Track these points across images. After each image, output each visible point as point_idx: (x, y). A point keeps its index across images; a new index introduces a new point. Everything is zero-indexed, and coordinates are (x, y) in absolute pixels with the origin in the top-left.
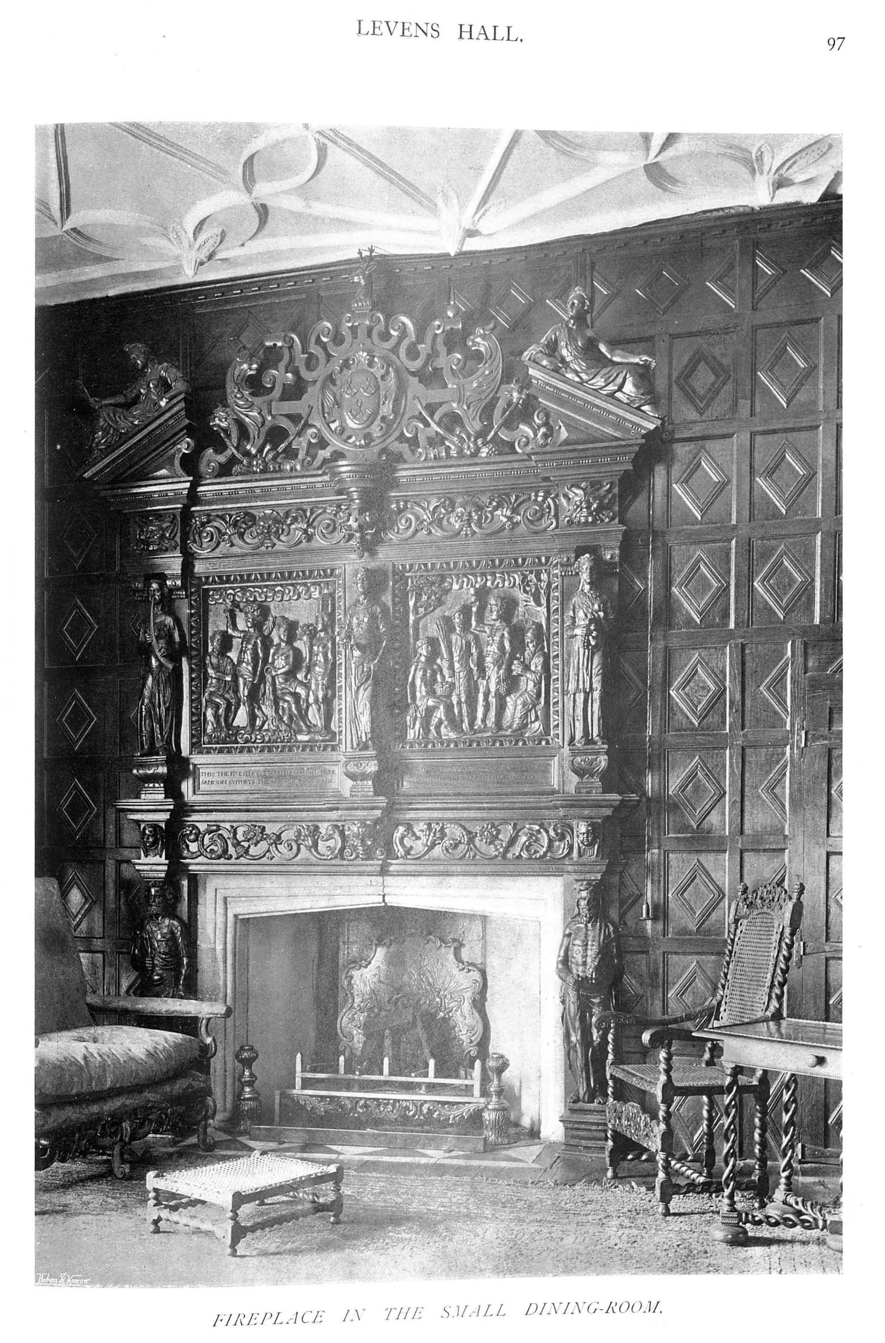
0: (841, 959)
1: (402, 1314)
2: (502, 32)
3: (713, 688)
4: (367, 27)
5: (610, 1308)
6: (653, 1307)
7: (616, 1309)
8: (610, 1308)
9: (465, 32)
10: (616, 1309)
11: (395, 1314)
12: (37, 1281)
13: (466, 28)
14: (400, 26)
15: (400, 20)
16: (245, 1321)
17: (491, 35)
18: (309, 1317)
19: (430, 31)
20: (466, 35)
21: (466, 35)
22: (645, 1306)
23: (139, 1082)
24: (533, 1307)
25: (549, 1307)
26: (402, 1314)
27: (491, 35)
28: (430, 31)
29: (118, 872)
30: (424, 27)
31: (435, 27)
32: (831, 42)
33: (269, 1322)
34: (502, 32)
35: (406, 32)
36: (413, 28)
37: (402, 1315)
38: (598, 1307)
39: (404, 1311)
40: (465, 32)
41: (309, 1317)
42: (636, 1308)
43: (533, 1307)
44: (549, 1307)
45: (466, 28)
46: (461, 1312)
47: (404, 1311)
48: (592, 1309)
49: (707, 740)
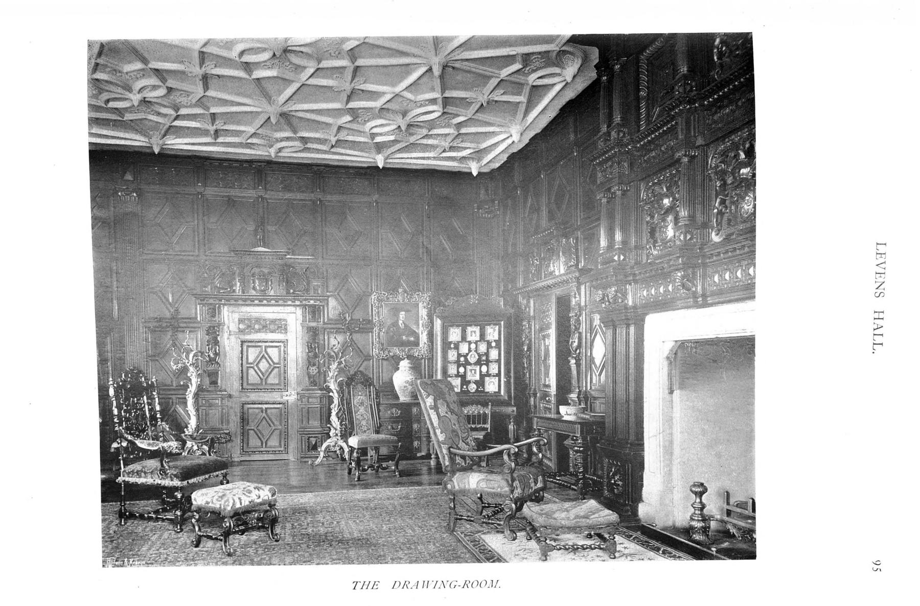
0: (93, 121)
1: (365, 585)
2: (878, 339)
4: (882, 249)
6: (493, 584)
7: (470, 585)
9: (879, 315)
10: (470, 585)
14: (883, 271)
15: (886, 271)
17: (877, 332)
19: (879, 291)
21: (876, 315)
24: (397, 584)
25: (439, 583)
26: (365, 585)
27: (877, 332)
28: (879, 291)
29: (564, 275)
34: (878, 339)
36: (881, 280)
37: (365, 587)
39: (367, 583)
40: (879, 315)
42: (483, 584)
43: (397, 584)
44: (439, 583)
46: (406, 584)
48: (452, 586)
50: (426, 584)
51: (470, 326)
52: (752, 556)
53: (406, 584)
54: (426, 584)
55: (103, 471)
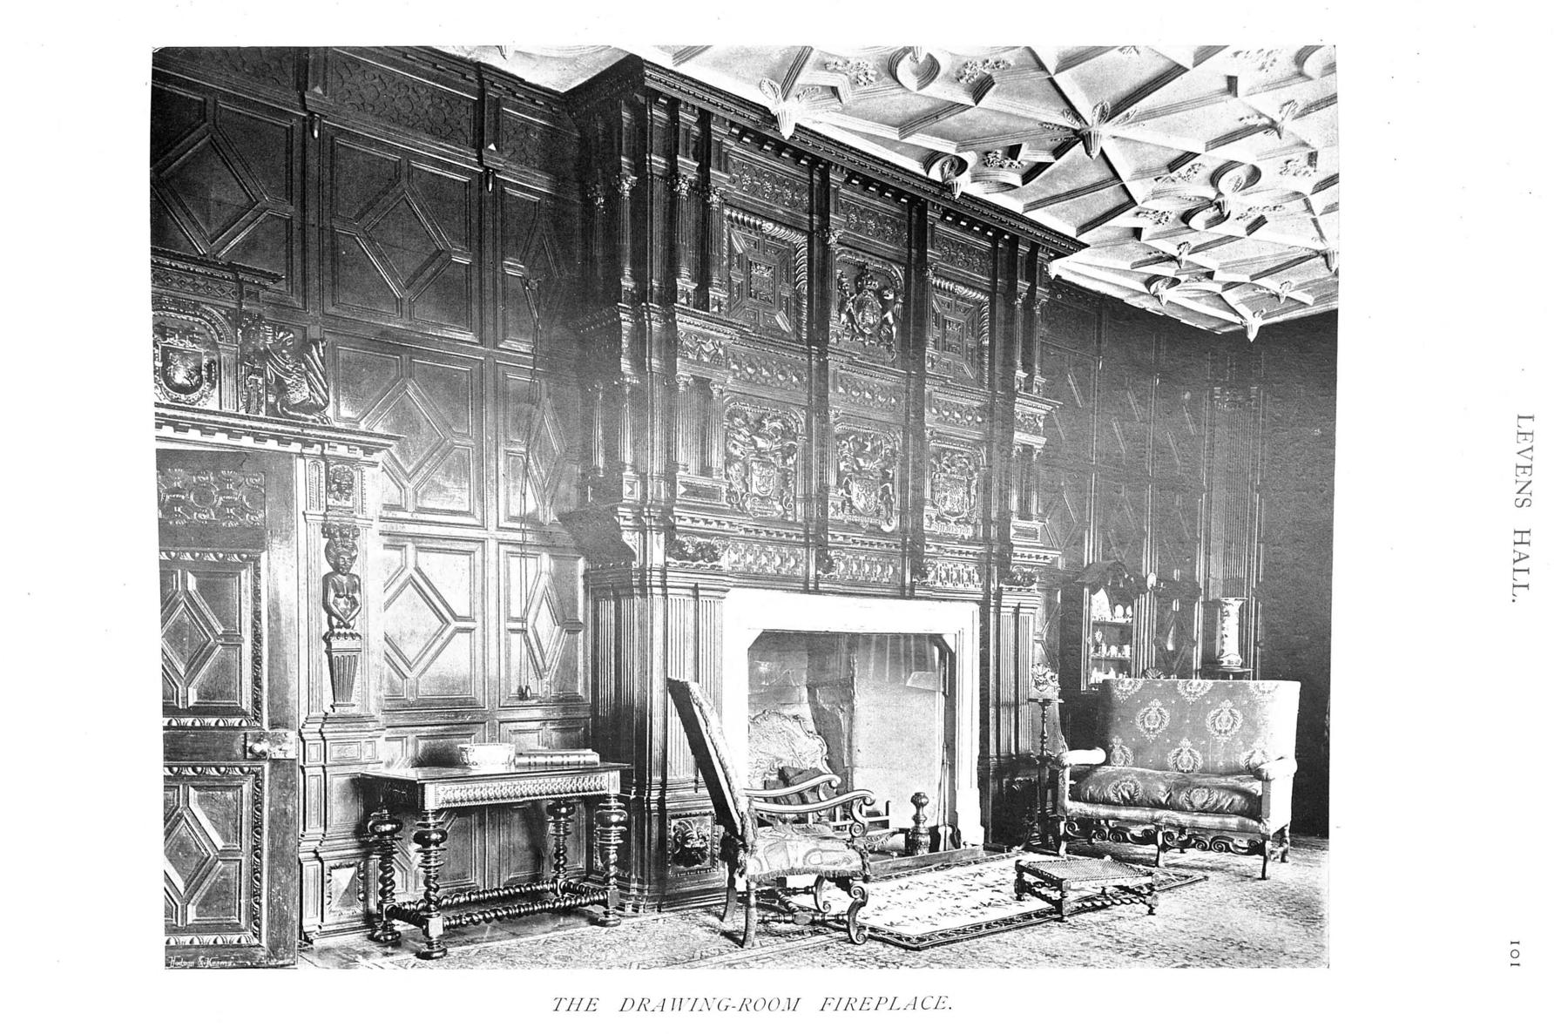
1: (574, 1005)
2: (1522, 578)
4: (1527, 426)
5: (744, 1005)
7: (751, 1007)
8: (744, 1005)
9: (1522, 536)
10: (751, 1007)
11: (565, 1005)
12: (168, 965)
13: (1526, 538)
16: (857, 1006)
17: (1519, 566)
18: (930, 1003)
19: (1522, 497)
20: (1518, 538)
21: (1518, 538)
22: (784, 1003)
23: (232, 751)
24: (629, 1003)
26: (574, 1005)
27: (1519, 566)
28: (1522, 497)
30: (1521, 486)
33: (884, 1008)
34: (1522, 578)
36: (1525, 478)
37: (574, 1007)
39: (576, 1001)
40: (1522, 536)
41: (930, 1003)
42: (775, 1004)
43: (629, 1003)
45: (1526, 538)
46: (643, 1005)
48: (722, 1007)
49: (1175, 732)
50: (678, 1004)
53: (643, 1005)
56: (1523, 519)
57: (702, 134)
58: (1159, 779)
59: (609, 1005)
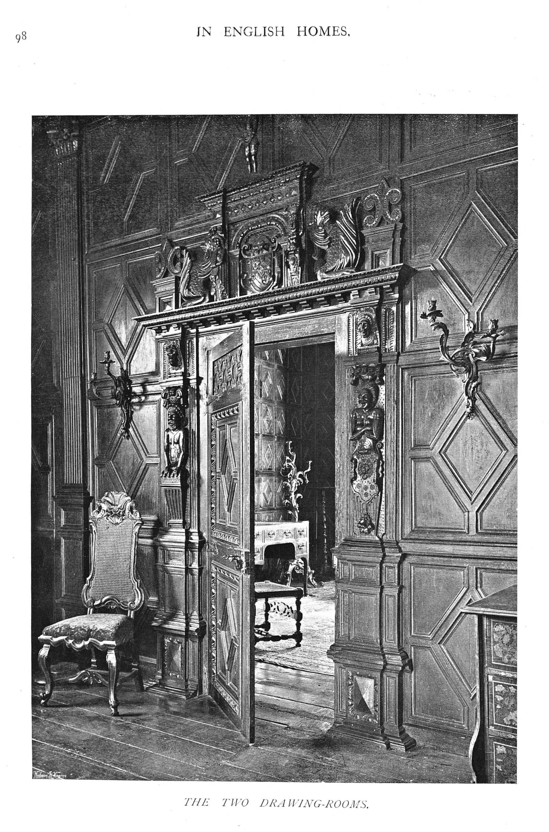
0: (515, 572)
1: (196, 802)
3: (404, 726)
5: (328, 805)
7: (333, 805)
8: (328, 805)
9: (304, 31)
10: (333, 805)
11: (191, 802)
13: (302, 29)
15: (332, 25)
20: (302, 34)
21: (302, 34)
24: (265, 802)
26: (196, 802)
30: (206, 33)
31: (344, 29)
32: (18, 37)
35: (336, 32)
36: (232, 30)
37: (196, 803)
38: (322, 803)
39: (197, 800)
40: (304, 31)
42: (345, 804)
45: (302, 29)
46: (273, 803)
47: (196, 803)
48: (317, 805)
50: (292, 803)
51: (184, 433)
52: (489, 762)
53: (273, 803)
54: (292, 803)
55: (504, 783)
56: (218, 32)
57: (93, 327)
58: (361, 430)
59: (255, 802)
